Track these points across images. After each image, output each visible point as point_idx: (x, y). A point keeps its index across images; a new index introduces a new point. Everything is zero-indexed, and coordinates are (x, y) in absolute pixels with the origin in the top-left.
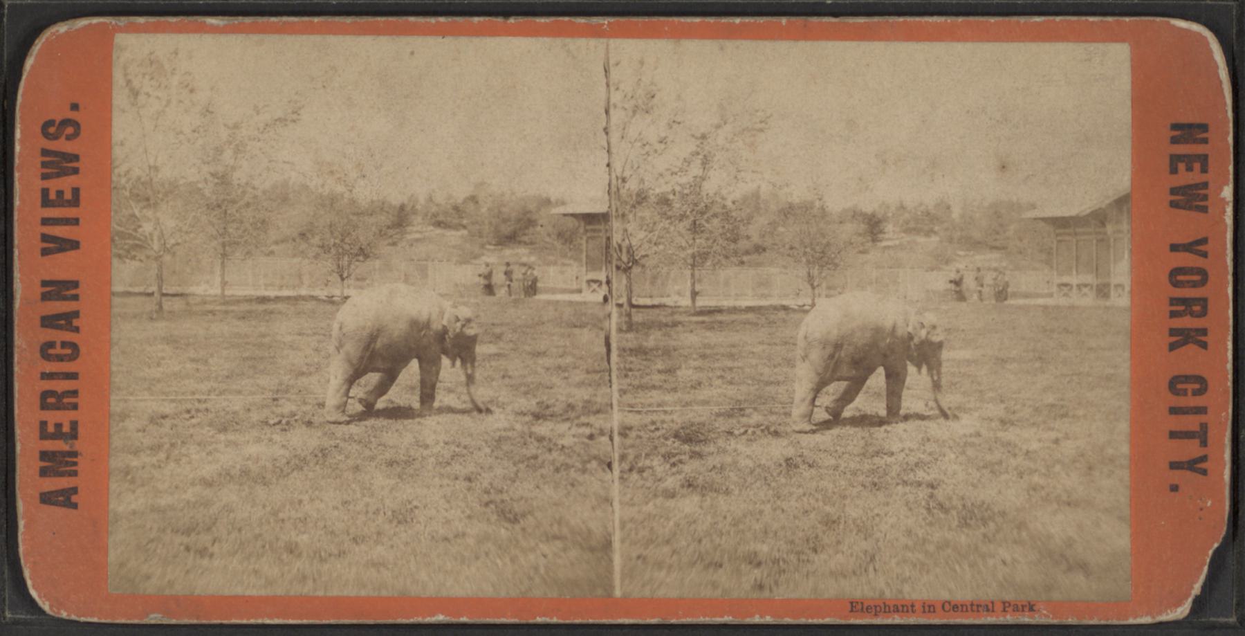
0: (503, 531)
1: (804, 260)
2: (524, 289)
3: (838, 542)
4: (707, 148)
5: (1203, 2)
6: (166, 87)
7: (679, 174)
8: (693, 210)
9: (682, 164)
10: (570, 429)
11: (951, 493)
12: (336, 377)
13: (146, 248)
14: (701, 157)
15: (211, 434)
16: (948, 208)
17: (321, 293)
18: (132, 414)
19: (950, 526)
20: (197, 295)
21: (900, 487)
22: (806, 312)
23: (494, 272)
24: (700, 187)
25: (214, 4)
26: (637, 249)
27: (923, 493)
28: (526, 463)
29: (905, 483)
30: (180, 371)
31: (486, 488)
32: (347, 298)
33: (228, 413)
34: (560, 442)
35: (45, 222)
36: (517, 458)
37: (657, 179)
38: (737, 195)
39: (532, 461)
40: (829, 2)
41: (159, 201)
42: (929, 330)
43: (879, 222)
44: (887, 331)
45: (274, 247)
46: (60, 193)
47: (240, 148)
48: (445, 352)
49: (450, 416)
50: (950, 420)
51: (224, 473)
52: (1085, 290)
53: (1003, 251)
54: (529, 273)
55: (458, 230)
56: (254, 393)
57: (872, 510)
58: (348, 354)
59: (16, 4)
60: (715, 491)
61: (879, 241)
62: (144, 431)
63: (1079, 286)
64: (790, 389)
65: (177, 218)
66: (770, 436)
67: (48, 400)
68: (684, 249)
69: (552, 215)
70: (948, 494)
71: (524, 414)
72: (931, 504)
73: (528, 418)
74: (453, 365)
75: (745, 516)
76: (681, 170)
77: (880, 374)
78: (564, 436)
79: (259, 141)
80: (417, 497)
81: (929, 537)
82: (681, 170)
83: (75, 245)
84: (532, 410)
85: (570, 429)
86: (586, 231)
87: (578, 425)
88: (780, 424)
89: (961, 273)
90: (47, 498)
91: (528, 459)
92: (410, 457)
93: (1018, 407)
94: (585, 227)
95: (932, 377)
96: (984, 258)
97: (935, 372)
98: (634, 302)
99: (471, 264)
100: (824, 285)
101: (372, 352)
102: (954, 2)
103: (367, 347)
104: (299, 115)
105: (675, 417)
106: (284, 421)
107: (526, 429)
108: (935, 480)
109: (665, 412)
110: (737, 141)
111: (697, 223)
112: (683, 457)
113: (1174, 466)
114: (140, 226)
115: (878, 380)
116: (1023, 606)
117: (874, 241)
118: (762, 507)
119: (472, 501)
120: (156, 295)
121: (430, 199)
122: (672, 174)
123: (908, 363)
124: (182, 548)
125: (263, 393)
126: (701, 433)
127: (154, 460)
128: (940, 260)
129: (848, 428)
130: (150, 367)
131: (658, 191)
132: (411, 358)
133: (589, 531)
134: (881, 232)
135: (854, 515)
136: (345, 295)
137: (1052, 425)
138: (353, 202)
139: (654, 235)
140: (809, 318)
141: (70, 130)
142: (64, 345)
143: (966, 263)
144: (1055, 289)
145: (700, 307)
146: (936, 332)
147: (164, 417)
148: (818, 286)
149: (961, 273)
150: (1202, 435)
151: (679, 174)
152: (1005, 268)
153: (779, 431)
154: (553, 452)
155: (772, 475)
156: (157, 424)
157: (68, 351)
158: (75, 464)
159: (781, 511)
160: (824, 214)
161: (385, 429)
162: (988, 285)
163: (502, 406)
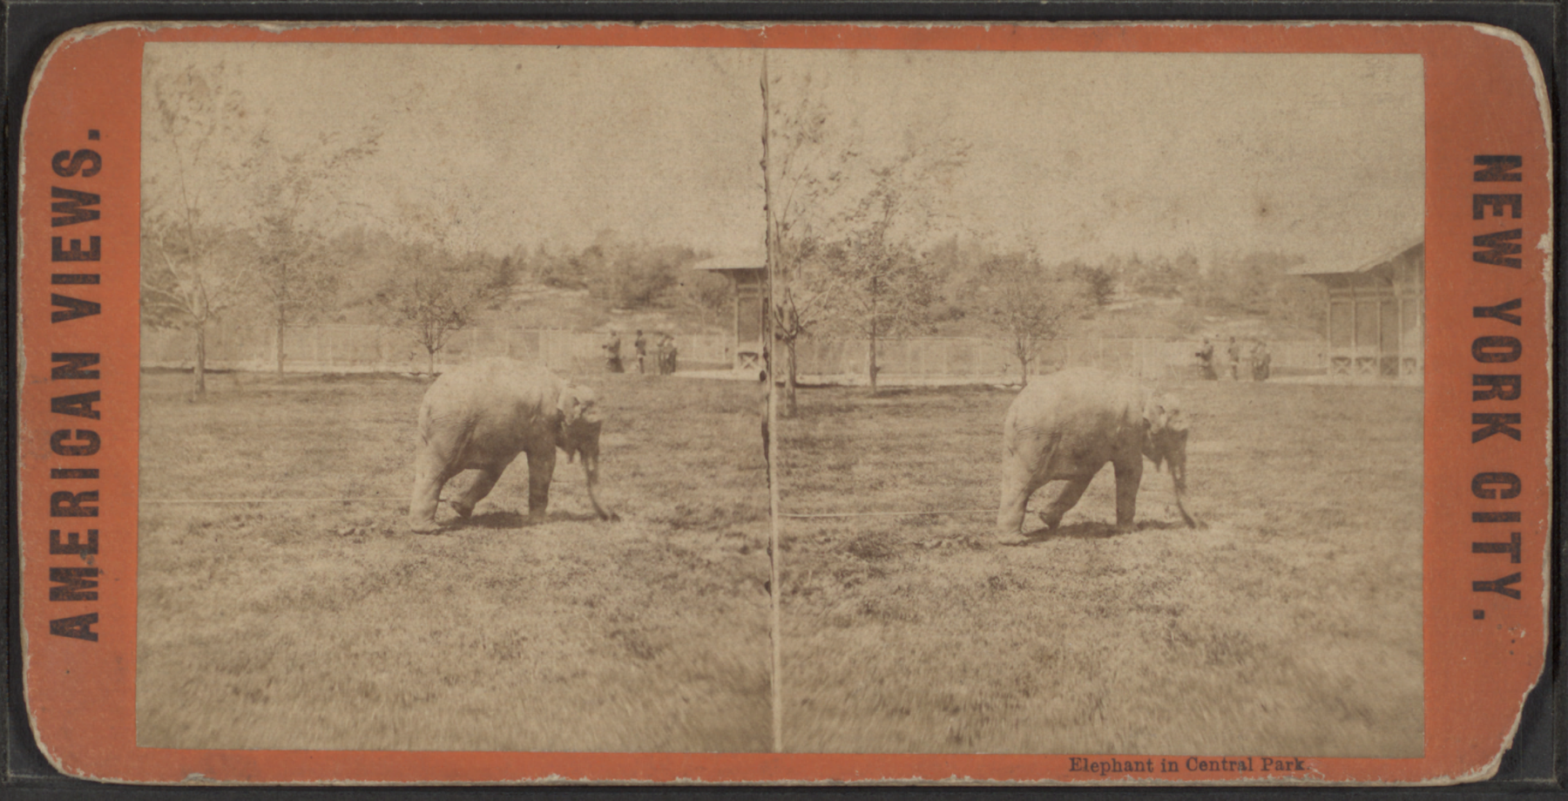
1: (1012, 327)
2: (660, 365)
3: (1056, 683)
5: (1515, 3)
7: (855, 219)
8: (873, 265)
9: (859, 207)
10: (717, 540)
14: (882, 197)
15: (265, 546)
18: (166, 522)
22: (1016, 393)
23: (623, 342)
24: (882, 236)
25: (269, 5)
26: (802, 314)
27: (1162, 622)
29: (1140, 608)
31: (612, 615)
32: (437, 375)
34: (706, 557)
35: (57, 279)
38: (336, 233)
39: (670, 581)
40: (1045, 2)
41: (200, 253)
42: (584, 407)
43: (1107, 280)
44: (1117, 417)
45: (345, 312)
46: (75, 243)
48: (561, 443)
49: (567, 524)
53: (1264, 317)
58: (438, 445)
59: (20, 5)
61: (1106, 303)
62: (182, 543)
63: (1359, 361)
64: (995, 490)
67: (61, 504)
68: (861, 313)
72: (1172, 634)
73: (665, 527)
74: (571, 460)
76: (858, 214)
77: (1108, 471)
79: (326, 177)
80: (525, 626)
81: (1170, 676)
82: (858, 214)
83: (94, 309)
86: (738, 291)
88: (982, 535)
89: (1211, 343)
90: (59, 628)
91: (665, 578)
93: (1282, 513)
95: (1174, 474)
97: (1177, 468)
99: (594, 332)
100: (1038, 359)
101: (469, 443)
102: (1201, 2)
103: (462, 438)
104: (965, 155)
106: (358, 531)
107: (662, 540)
108: (1178, 604)
110: (928, 178)
112: (860, 576)
113: (1479, 586)
115: (1105, 478)
119: (595, 631)
122: (846, 219)
123: (1144, 457)
124: (229, 690)
127: (194, 580)
128: (1184, 327)
129: (1068, 538)
134: (1110, 292)
135: (1076, 648)
136: (435, 371)
138: (445, 254)
140: (1019, 401)
141: (88, 164)
142: (81, 434)
143: (1215, 332)
144: (1328, 364)
147: (207, 525)
148: (1030, 360)
151: (855, 219)
154: (696, 570)
155: (972, 599)
156: (198, 534)
157: (86, 443)
158: (95, 584)
160: (1037, 269)
161: (485, 540)
163: (632, 511)
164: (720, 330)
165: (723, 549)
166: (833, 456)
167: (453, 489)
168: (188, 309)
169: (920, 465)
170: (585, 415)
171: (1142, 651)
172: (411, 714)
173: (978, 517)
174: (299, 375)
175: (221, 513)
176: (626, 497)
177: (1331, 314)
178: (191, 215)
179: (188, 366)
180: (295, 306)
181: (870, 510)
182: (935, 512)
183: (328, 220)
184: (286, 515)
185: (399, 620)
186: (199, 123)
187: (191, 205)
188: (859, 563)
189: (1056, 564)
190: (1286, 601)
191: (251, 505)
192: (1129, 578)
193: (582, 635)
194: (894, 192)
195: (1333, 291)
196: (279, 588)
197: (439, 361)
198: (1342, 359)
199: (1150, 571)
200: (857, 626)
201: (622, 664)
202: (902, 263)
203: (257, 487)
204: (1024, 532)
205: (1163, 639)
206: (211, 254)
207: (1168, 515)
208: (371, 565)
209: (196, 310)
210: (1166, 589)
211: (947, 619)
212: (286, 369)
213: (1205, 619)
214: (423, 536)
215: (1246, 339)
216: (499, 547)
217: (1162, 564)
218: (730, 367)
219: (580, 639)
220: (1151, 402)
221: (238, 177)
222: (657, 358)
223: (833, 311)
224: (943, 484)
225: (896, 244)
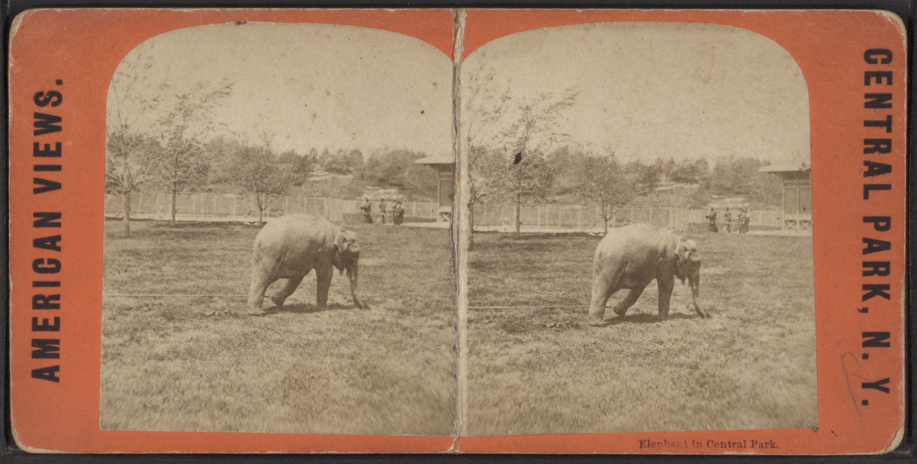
1: (600, 199)
3: (622, 407)
4: (530, 117)
6: (476, 79)
8: (176, 151)
9: (512, 128)
10: (426, 321)
12: (596, 292)
13: (118, 185)
14: (526, 123)
15: (163, 322)
16: (360, 154)
22: (601, 238)
23: (718, 214)
24: (524, 145)
26: (478, 190)
29: (671, 364)
32: (265, 223)
35: (37, 168)
36: (387, 343)
37: (493, 139)
38: (207, 141)
39: (398, 345)
41: (128, 151)
45: (211, 186)
46: (47, 146)
47: (531, 124)
48: (335, 263)
49: (681, 320)
50: (705, 319)
52: (806, 225)
53: (746, 196)
54: (397, 207)
55: (692, 184)
56: (195, 293)
58: (264, 264)
60: (193, 357)
62: (115, 319)
63: (801, 222)
64: (588, 294)
65: (141, 164)
66: (572, 329)
67: (40, 303)
69: (416, 164)
70: (364, 364)
71: (734, 318)
72: (352, 370)
73: (737, 322)
75: (553, 387)
76: (511, 133)
77: (654, 284)
79: (545, 119)
82: (511, 133)
83: (55, 186)
85: (767, 329)
87: (432, 319)
88: (580, 320)
89: (715, 211)
91: (395, 343)
93: (754, 310)
94: (439, 173)
95: (351, 277)
97: (694, 283)
98: (131, 217)
100: (614, 218)
101: (282, 263)
103: (278, 260)
104: (574, 100)
105: (503, 313)
106: (217, 314)
107: (394, 321)
109: (155, 298)
110: (552, 112)
111: (522, 171)
112: (168, 331)
113: (865, 386)
114: (114, 169)
115: (652, 288)
116: (766, 444)
117: (651, 186)
118: (567, 380)
119: (354, 374)
122: (161, 124)
123: (675, 276)
124: (141, 405)
125: (201, 293)
127: (121, 341)
128: (353, 193)
130: (119, 273)
131: (493, 148)
132: (311, 268)
135: (296, 376)
136: (263, 221)
139: (490, 180)
141: (55, 99)
142: (50, 261)
143: (374, 195)
144: (783, 224)
146: (696, 254)
147: (130, 309)
148: (609, 219)
150: (887, 124)
151: (509, 135)
152: (747, 208)
154: (754, 347)
156: (124, 314)
157: (53, 266)
159: (579, 383)
160: (614, 166)
163: (719, 312)
165: (429, 327)
169: (201, 267)
171: (672, 389)
172: (246, 421)
173: (578, 310)
177: (785, 194)
178: (124, 128)
180: (183, 182)
182: (553, 306)
184: (516, 316)
186: (129, 76)
187: (123, 123)
188: (508, 336)
189: (623, 338)
190: (757, 361)
191: (496, 310)
194: (532, 120)
199: (678, 342)
201: (707, 402)
202: (536, 161)
204: (605, 319)
206: (134, 152)
207: (688, 310)
209: (125, 184)
210: (687, 353)
211: (559, 369)
213: (370, 362)
215: (389, 200)
219: (345, 378)
220: (339, 234)
221: (151, 107)
222: (392, 215)
225: (189, 139)
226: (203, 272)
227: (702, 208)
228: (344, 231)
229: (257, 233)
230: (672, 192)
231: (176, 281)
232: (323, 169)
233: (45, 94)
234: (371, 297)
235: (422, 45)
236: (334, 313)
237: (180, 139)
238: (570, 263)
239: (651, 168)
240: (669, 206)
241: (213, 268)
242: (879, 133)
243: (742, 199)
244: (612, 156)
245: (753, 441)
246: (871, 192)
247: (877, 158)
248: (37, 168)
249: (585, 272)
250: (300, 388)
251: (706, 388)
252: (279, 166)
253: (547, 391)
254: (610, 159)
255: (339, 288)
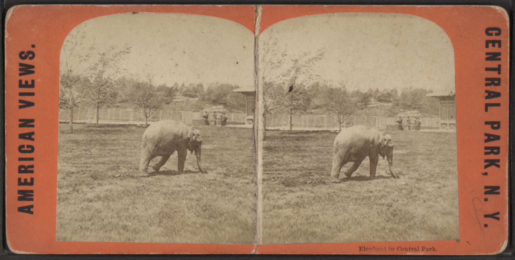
0: (400, 226)
1: (337, 112)
2: (221, 122)
3: (349, 228)
7: (286, 76)
8: (99, 84)
9: (287, 72)
10: (239, 180)
11: (206, 204)
14: (295, 69)
16: (202, 86)
17: (139, 123)
18: (60, 172)
19: (205, 217)
20: (280, 130)
21: (375, 206)
22: (337, 133)
24: (294, 81)
28: (412, 199)
29: (377, 204)
30: (80, 155)
31: (394, 209)
32: (149, 125)
33: (98, 172)
34: (236, 185)
35: (21, 94)
38: (116, 79)
39: (224, 193)
41: (72, 85)
42: (196, 136)
44: (370, 141)
45: (119, 104)
46: (27, 82)
48: (188, 148)
49: (382, 180)
51: (97, 197)
52: (452, 126)
53: (419, 110)
54: (223, 116)
55: (389, 103)
57: (363, 215)
58: (148, 148)
62: (64, 179)
63: (450, 124)
64: (330, 165)
66: (321, 184)
67: (23, 170)
68: (95, 100)
70: (204, 204)
73: (413, 181)
74: (384, 158)
75: (311, 217)
77: (367, 159)
78: (429, 187)
79: (306, 67)
80: (176, 208)
82: (287, 74)
83: (31, 104)
84: (224, 172)
85: (431, 184)
88: (326, 179)
89: (402, 118)
91: (222, 192)
92: (173, 191)
93: (424, 174)
96: (409, 113)
97: (390, 159)
100: (345, 122)
103: (156, 146)
105: (283, 175)
106: (122, 176)
107: (221, 180)
108: (389, 203)
110: (310, 63)
111: (293, 96)
112: (95, 185)
113: (486, 216)
114: (64, 95)
115: (366, 161)
116: (430, 249)
117: (366, 104)
118: (318, 213)
119: (199, 209)
120: (70, 123)
121: (183, 85)
122: (91, 69)
123: (379, 155)
124: (79, 227)
126: (293, 183)
127: (68, 191)
128: (198, 108)
129: (162, 175)
130: (67, 153)
131: (277, 83)
133: (436, 227)
134: (174, 95)
135: (166, 211)
136: (148, 124)
137: (246, 177)
139: (275, 101)
140: (338, 135)
141: (31, 55)
142: (28, 146)
143: (210, 109)
144: (440, 125)
145: (294, 131)
146: (391, 142)
147: (73, 173)
148: (342, 123)
149: (208, 113)
150: (498, 69)
151: (286, 76)
152: (419, 117)
153: (134, 176)
154: (423, 194)
155: (131, 194)
156: (70, 176)
159: (325, 215)
161: (163, 179)
162: (218, 119)
163: (404, 175)
164: (435, 116)
166: (85, 146)
167: (153, 162)
168: (68, 102)
170: (197, 138)
171: (377, 218)
172: (138, 236)
174: (103, 125)
175: (77, 169)
176: (210, 165)
177: (441, 109)
178: (69, 72)
179: (68, 122)
180: (103, 102)
181: (97, 164)
182: (310, 172)
183: (113, 74)
184: (290, 177)
185: (325, 211)
187: (69, 69)
188: (285, 188)
192: (182, 189)
193: (384, 215)
195: (441, 102)
196: (286, 201)
197: (149, 121)
198: (444, 124)
200: (94, 202)
201: (397, 225)
202: (301, 90)
203: (89, 161)
204: (340, 179)
205: (194, 209)
206: (75, 85)
208: (126, 187)
212: (293, 129)
214: (335, 184)
216: (168, 182)
217: (384, 190)
218: (438, 128)
219: (194, 212)
220: (190, 131)
223: (85, 99)
224: (313, 163)
225: (106, 77)
226: (114, 152)
227: (394, 117)
228: (193, 130)
229: (145, 130)
230: (377, 107)
231: (99, 157)
232: (181, 94)
233: (25, 52)
234: (209, 166)
235: (237, 25)
236: (187, 175)
237: (101, 78)
238: (320, 147)
239: (366, 94)
240: (375, 115)
241: (120, 150)
242: (494, 75)
243: (417, 112)
244: (344, 87)
245: (423, 247)
246: (489, 108)
247: (492, 88)
248: (21, 94)
249: (328, 153)
250: (358, 224)
251: (396, 218)
252: (157, 93)
253: (307, 219)
254: (343, 89)
255: (190, 161)
